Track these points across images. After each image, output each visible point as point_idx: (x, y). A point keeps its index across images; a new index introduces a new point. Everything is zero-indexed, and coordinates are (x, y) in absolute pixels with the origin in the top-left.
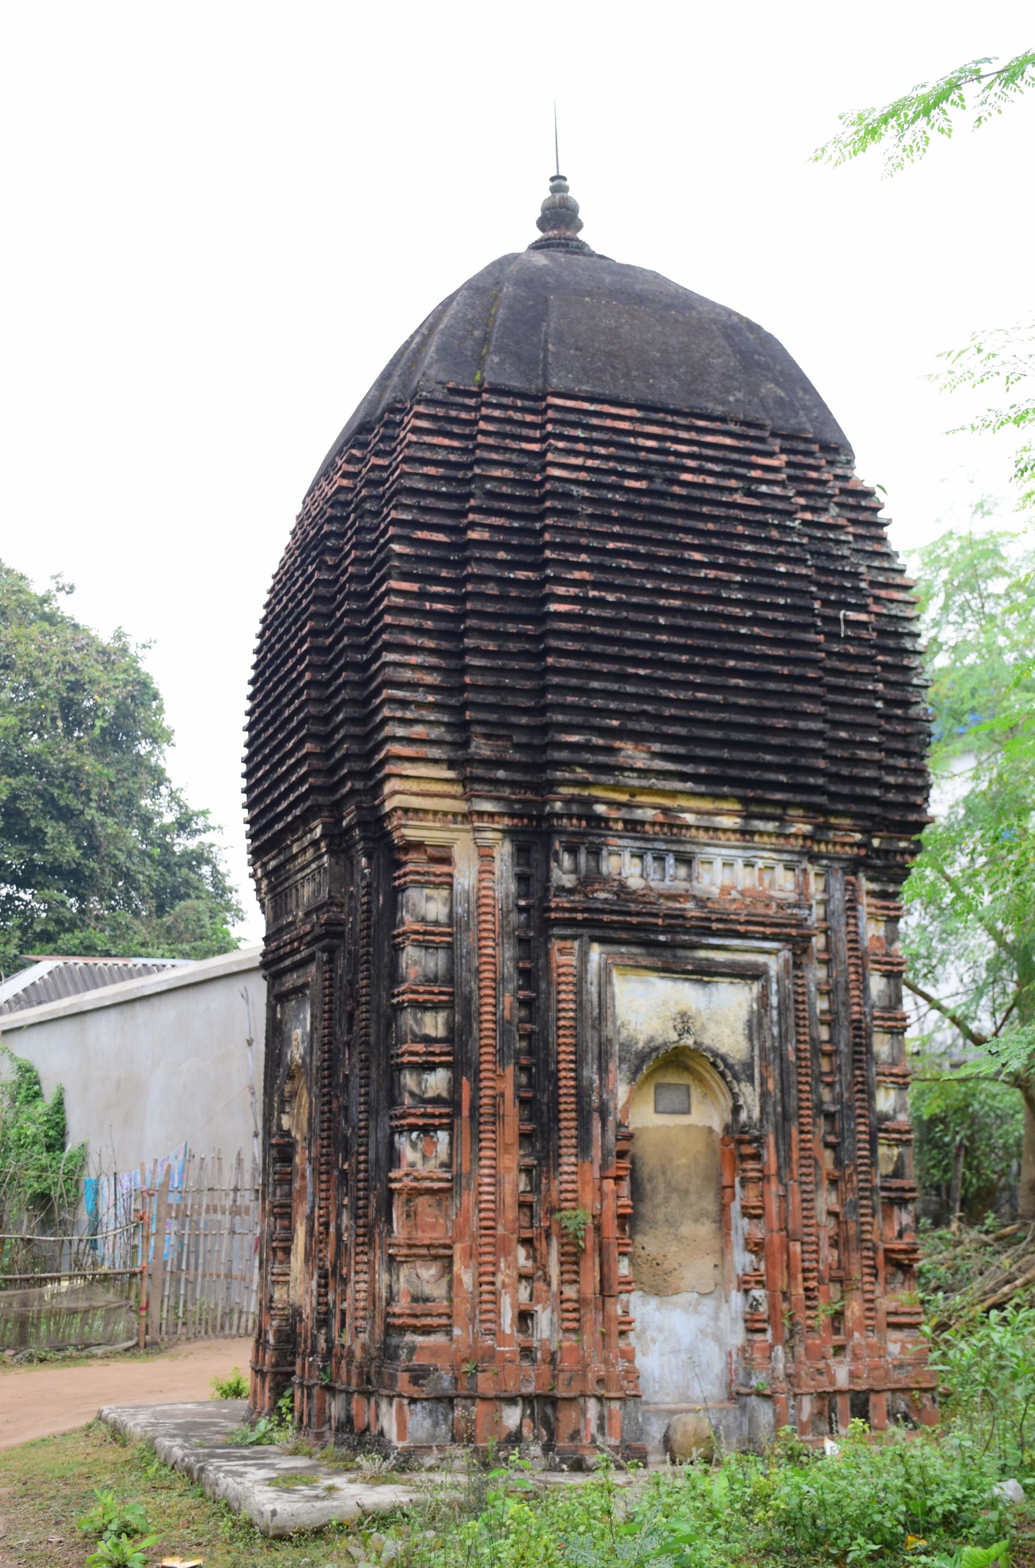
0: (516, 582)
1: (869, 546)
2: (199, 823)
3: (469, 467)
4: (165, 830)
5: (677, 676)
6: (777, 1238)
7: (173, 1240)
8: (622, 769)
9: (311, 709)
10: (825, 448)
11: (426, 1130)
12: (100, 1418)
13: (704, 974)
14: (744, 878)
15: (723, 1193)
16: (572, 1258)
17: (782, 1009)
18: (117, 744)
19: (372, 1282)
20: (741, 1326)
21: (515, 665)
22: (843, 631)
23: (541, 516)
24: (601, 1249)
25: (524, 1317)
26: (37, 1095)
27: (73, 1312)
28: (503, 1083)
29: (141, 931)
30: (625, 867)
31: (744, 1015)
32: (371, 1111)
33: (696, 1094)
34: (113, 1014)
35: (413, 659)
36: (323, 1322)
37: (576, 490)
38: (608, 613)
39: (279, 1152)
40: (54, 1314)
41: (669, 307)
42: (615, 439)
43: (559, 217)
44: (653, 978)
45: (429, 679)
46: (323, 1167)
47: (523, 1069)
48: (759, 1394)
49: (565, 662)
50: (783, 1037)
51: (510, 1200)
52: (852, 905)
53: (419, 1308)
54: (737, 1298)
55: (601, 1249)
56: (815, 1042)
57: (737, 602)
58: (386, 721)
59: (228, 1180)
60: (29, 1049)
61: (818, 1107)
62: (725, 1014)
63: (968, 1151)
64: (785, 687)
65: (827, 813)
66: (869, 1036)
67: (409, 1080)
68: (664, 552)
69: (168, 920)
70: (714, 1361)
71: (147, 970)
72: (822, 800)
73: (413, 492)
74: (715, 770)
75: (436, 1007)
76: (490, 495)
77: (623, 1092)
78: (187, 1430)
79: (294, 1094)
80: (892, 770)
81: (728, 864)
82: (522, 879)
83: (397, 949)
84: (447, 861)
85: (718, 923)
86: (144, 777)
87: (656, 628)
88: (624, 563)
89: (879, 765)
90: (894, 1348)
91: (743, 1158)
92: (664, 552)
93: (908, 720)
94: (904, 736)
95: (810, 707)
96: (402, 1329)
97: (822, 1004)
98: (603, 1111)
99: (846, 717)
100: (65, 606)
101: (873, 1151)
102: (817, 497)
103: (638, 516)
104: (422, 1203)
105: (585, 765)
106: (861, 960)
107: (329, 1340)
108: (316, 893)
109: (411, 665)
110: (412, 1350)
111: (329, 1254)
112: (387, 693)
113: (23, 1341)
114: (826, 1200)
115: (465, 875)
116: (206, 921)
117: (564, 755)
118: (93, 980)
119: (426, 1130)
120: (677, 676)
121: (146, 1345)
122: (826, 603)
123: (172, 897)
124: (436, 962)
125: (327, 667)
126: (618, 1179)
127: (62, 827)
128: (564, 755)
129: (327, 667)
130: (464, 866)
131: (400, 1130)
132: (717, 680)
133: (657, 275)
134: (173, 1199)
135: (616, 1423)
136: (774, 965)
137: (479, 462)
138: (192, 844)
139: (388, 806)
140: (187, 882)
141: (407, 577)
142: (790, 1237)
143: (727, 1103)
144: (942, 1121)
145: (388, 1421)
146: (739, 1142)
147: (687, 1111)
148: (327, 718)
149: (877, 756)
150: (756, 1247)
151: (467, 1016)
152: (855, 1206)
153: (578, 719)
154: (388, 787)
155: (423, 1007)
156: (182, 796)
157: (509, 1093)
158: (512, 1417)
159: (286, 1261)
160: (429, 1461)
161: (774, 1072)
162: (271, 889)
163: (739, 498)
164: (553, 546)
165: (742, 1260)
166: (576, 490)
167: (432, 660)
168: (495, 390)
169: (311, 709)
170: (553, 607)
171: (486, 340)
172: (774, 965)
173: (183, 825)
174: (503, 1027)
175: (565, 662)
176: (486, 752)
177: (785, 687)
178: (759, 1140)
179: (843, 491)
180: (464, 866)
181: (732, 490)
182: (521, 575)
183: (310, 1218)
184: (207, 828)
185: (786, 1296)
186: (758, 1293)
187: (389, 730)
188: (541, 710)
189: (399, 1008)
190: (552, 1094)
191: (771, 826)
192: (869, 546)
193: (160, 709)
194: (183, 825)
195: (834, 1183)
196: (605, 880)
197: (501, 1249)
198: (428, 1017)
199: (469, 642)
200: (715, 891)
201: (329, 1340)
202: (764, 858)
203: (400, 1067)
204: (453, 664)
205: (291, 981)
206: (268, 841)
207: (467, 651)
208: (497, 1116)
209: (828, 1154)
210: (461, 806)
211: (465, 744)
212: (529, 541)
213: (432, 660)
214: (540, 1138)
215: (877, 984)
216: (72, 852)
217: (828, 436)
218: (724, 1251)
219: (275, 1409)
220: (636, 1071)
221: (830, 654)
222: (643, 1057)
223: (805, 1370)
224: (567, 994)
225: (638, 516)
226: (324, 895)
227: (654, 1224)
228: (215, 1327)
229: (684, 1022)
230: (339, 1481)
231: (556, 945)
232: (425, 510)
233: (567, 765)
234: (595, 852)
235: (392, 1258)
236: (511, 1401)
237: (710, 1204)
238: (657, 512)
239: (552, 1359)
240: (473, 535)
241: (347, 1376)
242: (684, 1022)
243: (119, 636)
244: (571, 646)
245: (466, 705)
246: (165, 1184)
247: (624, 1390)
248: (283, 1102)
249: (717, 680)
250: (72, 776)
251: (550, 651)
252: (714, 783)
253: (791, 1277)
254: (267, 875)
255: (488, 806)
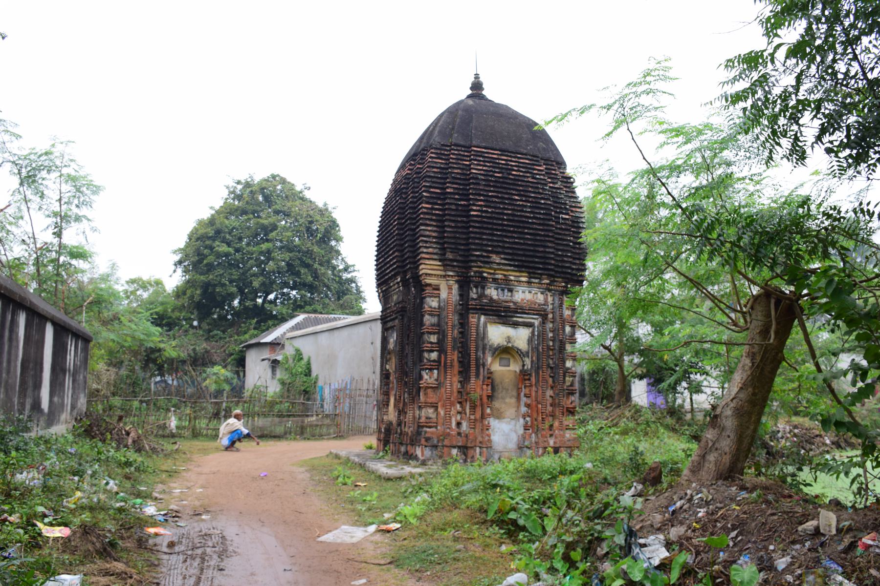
0: (461, 205)
1: (570, 195)
2: (351, 269)
3: (447, 169)
4: (340, 271)
5: (509, 234)
6: (534, 403)
7: (348, 405)
8: (492, 263)
9: (397, 242)
10: (558, 163)
11: (431, 370)
12: (331, 453)
13: (515, 325)
14: (528, 296)
15: (519, 390)
16: (473, 408)
17: (538, 336)
18: (324, 242)
19: (414, 413)
20: (522, 428)
21: (460, 230)
22: (561, 221)
23: (469, 185)
24: (482, 405)
25: (459, 424)
26: (302, 359)
27: (317, 426)
28: (454, 357)
29: (333, 306)
30: (492, 292)
31: (527, 337)
32: (414, 364)
33: (512, 361)
34: (326, 334)
35: (429, 228)
36: (399, 424)
37: (480, 177)
38: (489, 215)
39: (385, 376)
40: (311, 426)
41: (510, 118)
42: (492, 161)
43: (477, 86)
44: (500, 326)
45: (434, 234)
46: (400, 380)
47: (460, 352)
48: (527, 447)
49: (475, 230)
50: (538, 344)
51: (455, 390)
52: (561, 305)
53: (428, 421)
54: (522, 420)
55: (482, 405)
56: (548, 346)
57: (529, 212)
58: (421, 247)
59: (365, 387)
60: (298, 344)
61: (548, 366)
62: (521, 337)
63: (604, 383)
64: (542, 238)
65: (554, 277)
66: (565, 344)
67: (426, 355)
68: (506, 196)
69: (341, 302)
70: (514, 438)
71: (335, 319)
72: (553, 273)
73: (430, 177)
74: (520, 263)
75: (434, 333)
76: (453, 178)
77: (489, 359)
78: (358, 455)
79: (390, 359)
80: (575, 264)
81: (523, 292)
82: (461, 295)
83: (423, 316)
84: (438, 289)
85: (520, 310)
86: (334, 254)
87: (503, 220)
88: (494, 199)
89: (571, 262)
90: (568, 436)
91: (525, 380)
92: (506, 196)
93: (580, 249)
94: (579, 254)
95: (550, 245)
96: (423, 427)
97: (551, 335)
98: (484, 365)
99: (561, 248)
100: (307, 194)
101: (564, 379)
102: (554, 179)
103: (499, 185)
104: (429, 391)
105: (481, 262)
106: (563, 322)
107: (401, 430)
108: (398, 298)
109: (428, 230)
110: (426, 432)
111: (401, 405)
112: (421, 238)
113: (302, 433)
114: (549, 393)
115: (444, 294)
116: (354, 302)
117: (474, 258)
118: (317, 322)
119: (431, 370)
120: (509, 234)
121: (340, 436)
122: (556, 212)
123: (344, 295)
124: (434, 320)
125: (402, 229)
126: (487, 385)
127: (306, 270)
128: (474, 258)
129: (402, 229)
130: (443, 292)
131: (423, 369)
132: (522, 236)
133: (507, 107)
134: (348, 392)
135: (485, 454)
136: (536, 323)
137: (450, 168)
138: (349, 276)
139: (421, 273)
140: (347, 289)
141: (427, 203)
142: (538, 403)
143: (521, 363)
144: (597, 373)
145: (418, 452)
146: (524, 375)
147: (509, 366)
148: (402, 245)
149: (570, 260)
150: (528, 406)
151: (444, 336)
152: (558, 394)
153: (479, 247)
154: (421, 267)
155: (430, 333)
156: (346, 260)
157: (456, 359)
158: (455, 452)
159: (387, 408)
160: (430, 463)
161: (535, 354)
162: (383, 296)
163: (530, 179)
164: (472, 194)
165: (524, 409)
166: (480, 177)
167: (435, 229)
168: (456, 145)
169: (397, 242)
170: (472, 213)
171: (453, 129)
172: (536, 323)
173: (346, 269)
174: (454, 339)
175: (475, 230)
176: (451, 257)
177: (542, 238)
178: (530, 375)
179: (563, 177)
180: (443, 292)
181: (528, 177)
182: (462, 203)
183: (395, 395)
184: (354, 271)
185: (536, 420)
186: (528, 419)
187: (421, 250)
188: (468, 244)
189: (423, 333)
190: (468, 358)
191: (537, 281)
192: (570, 195)
193: (339, 230)
194: (346, 269)
195: (552, 388)
196: (486, 296)
197: (452, 404)
198: (432, 336)
199: (446, 223)
200: (519, 300)
201: (401, 430)
202: (534, 290)
203: (423, 351)
204: (441, 230)
205: (390, 324)
206: (382, 281)
207: (446, 226)
208: (452, 366)
209: (551, 379)
210: (443, 273)
211: (445, 254)
212: (465, 192)
213: (435, 229)
214: (465, 374)
215: (568, 329)
216: (310, 279)
217: (559, 159)
218: (518, 407)
219: (384, 449)
220: (494, 353)
221: (557, 228)
222: (496, 349)
223: (541, 440)
224: (473, 331)
225: (499, 185)
226: (401, 299)
227: (498, 398)
228: (362, 432)
229: (509, 339)
230: (405, 467)
231: (471, 315)
232: (433, 182)
233: (475, 261)
234: (483, 288)
235: (420, 407)
236: (454, 447)
237: (515, 393)
238: (505, 184)
239: (466, 436)
240: (448, 190)
241: (406, 440)
242: (509, 339)
243: (325, 205)
244: (477, 225)
245: (445, 243)
246: (346, 387)
247: (487, 445)
248: (387, 361)
249: (522, 236)
250: (309, 253)
251: (471, 226)
252: (520, 268)
253: (538, 414)
254: (382, 292)
255: (451, 273)
